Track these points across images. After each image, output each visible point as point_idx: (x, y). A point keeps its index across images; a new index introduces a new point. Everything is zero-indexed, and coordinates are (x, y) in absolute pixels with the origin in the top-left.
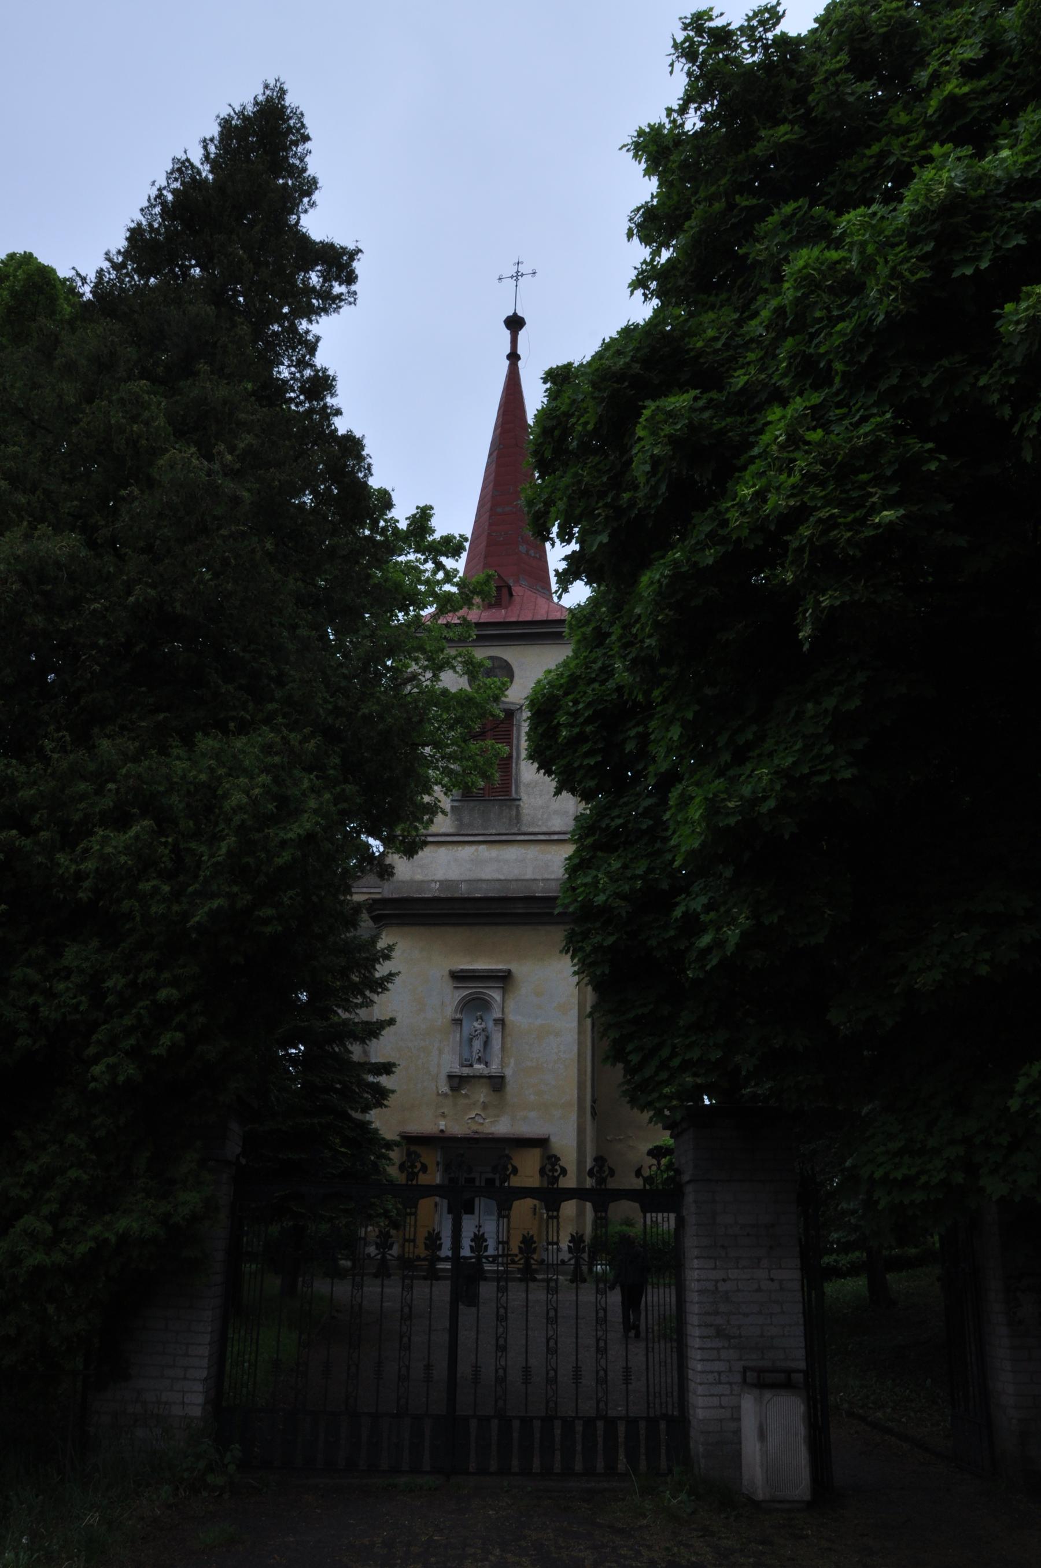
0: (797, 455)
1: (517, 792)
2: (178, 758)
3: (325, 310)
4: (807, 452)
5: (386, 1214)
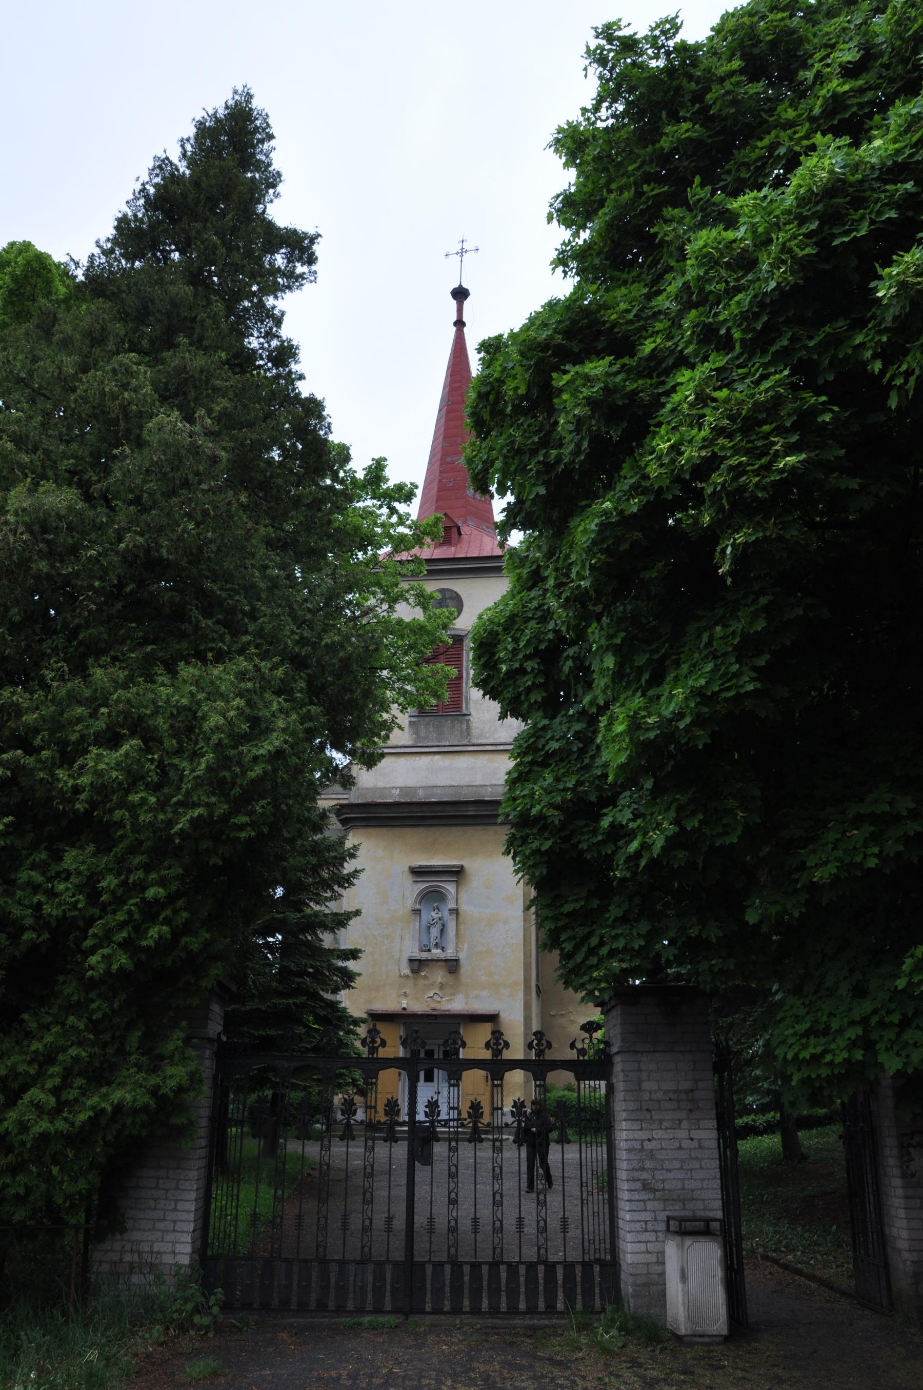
0: (707, 411)
1: (467, 708)
2: (163, 684)
3: (289, 288)
4: (714, 408)
5: (354, 1083)
